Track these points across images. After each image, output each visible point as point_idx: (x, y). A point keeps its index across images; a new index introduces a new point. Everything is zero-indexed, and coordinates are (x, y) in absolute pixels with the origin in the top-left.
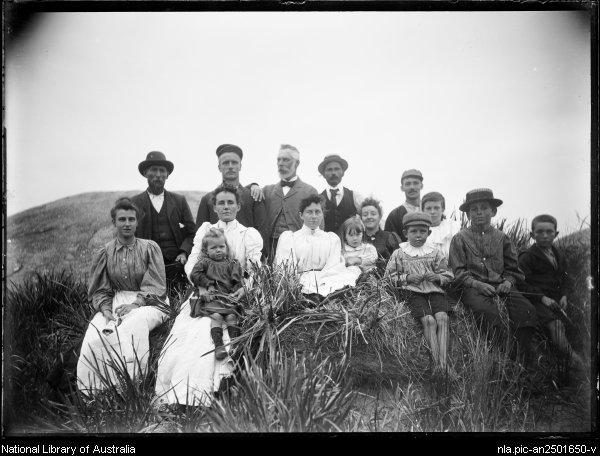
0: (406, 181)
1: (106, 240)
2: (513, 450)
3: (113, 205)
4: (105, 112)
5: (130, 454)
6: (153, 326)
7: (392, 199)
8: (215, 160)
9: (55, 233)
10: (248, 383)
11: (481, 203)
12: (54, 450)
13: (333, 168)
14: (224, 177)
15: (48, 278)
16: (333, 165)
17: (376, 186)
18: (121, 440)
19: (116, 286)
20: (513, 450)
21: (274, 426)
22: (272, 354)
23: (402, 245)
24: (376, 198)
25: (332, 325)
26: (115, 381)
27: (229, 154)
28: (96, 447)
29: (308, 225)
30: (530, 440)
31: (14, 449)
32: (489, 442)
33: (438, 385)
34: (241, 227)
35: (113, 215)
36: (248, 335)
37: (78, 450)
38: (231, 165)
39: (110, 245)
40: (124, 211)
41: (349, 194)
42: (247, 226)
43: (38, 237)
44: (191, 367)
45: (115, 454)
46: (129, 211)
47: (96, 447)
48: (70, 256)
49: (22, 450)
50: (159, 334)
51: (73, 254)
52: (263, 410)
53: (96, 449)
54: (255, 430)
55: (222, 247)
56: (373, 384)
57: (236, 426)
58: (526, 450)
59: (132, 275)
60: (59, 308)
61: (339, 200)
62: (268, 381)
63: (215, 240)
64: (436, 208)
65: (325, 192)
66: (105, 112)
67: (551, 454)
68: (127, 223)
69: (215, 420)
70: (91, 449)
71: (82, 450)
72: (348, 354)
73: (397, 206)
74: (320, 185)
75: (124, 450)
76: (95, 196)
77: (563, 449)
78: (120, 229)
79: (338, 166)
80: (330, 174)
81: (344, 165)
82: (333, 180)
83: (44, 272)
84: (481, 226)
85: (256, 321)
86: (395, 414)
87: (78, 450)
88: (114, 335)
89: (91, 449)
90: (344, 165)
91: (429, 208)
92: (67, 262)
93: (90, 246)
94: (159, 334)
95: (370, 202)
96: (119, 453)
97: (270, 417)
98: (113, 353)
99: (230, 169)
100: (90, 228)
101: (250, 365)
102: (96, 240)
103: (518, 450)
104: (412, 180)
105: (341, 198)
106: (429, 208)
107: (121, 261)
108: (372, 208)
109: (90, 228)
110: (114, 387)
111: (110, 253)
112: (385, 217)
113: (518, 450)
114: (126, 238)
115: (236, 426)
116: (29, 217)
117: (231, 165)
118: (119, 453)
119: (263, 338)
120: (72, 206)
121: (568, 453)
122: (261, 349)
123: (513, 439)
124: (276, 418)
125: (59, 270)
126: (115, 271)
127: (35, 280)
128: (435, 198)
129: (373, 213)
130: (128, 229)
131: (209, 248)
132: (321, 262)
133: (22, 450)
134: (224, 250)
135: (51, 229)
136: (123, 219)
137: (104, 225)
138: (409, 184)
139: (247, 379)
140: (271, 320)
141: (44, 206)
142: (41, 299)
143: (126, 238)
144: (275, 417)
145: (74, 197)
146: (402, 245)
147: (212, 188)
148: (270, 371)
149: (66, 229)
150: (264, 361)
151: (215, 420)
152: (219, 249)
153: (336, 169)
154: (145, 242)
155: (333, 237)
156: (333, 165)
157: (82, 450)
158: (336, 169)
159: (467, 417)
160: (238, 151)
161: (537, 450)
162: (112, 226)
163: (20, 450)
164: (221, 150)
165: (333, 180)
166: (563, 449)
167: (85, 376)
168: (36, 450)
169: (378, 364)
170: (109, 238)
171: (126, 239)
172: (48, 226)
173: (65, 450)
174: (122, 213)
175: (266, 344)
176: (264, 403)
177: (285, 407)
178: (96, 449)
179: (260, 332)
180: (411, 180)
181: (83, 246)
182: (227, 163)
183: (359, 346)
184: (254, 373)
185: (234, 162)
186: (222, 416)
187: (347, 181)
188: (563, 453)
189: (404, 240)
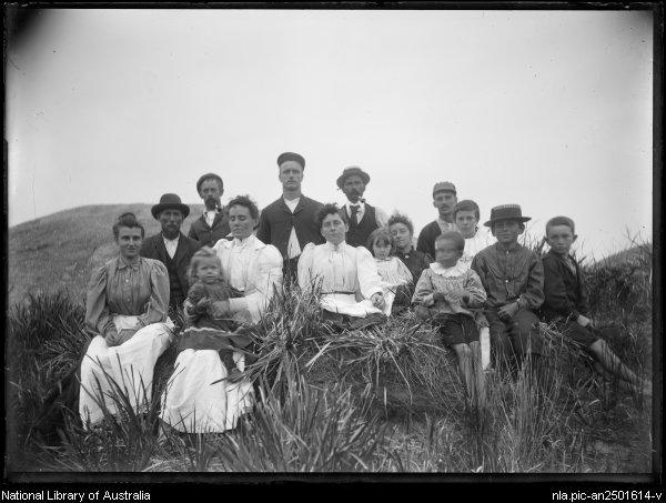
0: (437, 196)
1: (107, 258)
2: (569, 496)
3: (114, 220)
4: (116, 123)
5: (144, 501)
6: (158, 353)
7: (423, 215)
8: (276, 170)
9: (50, 250)
10: (264, 416)
11: (509, 219)
12: (59, 496)
13: (353, 181)
14: (284, 187)
15: (43, 300)
16: (354, 179)
17: (403, 197)
18: (133, 482)
19: (113, 308)
20: (569, 496)
21: (293, 464)
22: (292, 384)
23: (432, 265)
24: (402, 213)
25: (355, 351)
26: (113, 410)
27: (291, 165)
28: (107, 493)
29: (332, 241)
30: (589, 486)
31: (15, 496)
32: (542, 487)
33: (475, 423)
34: (260, 244)
35: (116, 232)
36: (264, 363)
37: (86, 496)
38: (291, 174)
39: (111, 263)
40: (128, 229)
41: (370, 211)
42: (355, 246)
43: (31, 255)
44: (207, 395)
45: (128, 501)
46: (134, 229)
47: (107, 493)
48: (67, 276)
49: (25, 496)
50: (165, 364)
51: (70, 273)
52: (280, 446)
53: (107, 495)
54: (271, 468)
55: (213, 267)
56: (402, 417)
57: (251, 463)
58: (583, 496)
59: (135, 299)
60: (61, 330)
61: (359, 218)
62: (285, 417)
63: (207, 259)
64: (469, 218)
65: (345, 207)
66: (116, 123)
67: (612, 501)
68: (131, 242)
69: (227, 456)
70: (101, 495)
71: (92, 496)
72: (374, 381)
73: (432, 221)
74: (341, 200)
75: (138, 496)
76: (96, 209)
77: (626, 496)
78: (123, 247)
79: (359, 179)
80: (350, 188)
81: (365, 178)
82: (354, 195)
83: (38, 293)
84: (507, 244)
85: (272, 347)
86: (416, 454)
87: (86, 496)
88: (118, 359)
89: (101, 495)
90: (365, 178)
91: (461, 219)
92: (64, 283)
93: (88, 265)
94: (165, 364)
95: (396, 219)
96: (132, 500)
97: (288, 453)
98: (114, 386)
99: (291, 178)
100: (91, 245)
101: (266, 395)
102: (95, 258)
103: (574, 496)
104: (444, 194)
105: (362, 215)
106: (461, 219)
107: (123, 282)
108: (399, 225)
109: (91, 245)
110: (114, 418)
111: (112, 273)
112: (417, 234)
113: (574, 496)
114: (130, 258)
115: (251, 463)
116: (21, 232)
117: (291, 174)
118: (132, 500)
119: (280, 368)
120: (69, 220)
121: (630, 500)
122: (278, 378)
123: (570, 484)
124: (295, 455)
125: (53, 291)
126: (115, 293)
127: (28, 303)
128: (470, 207)
129: (402, 231)
130: (132, 248)
131: (199, 268)
132: (358, 283)
133: (25, 496)
134: (216, 273)
135: (46, 246)
136: (127, 238)
137: (104, 242)
138: (440, 199)
139: (262, 412)
140: (289, 347)
141: (37, 221)
142: (34, 323)
143: (130, 258)
144: (294, 454)
145: (71, 211)
146: (432, 265)
147: (278, 196)
148: (288, 403)
149: (62, 245)
150: (282, 392)
151: (227, 456)
152: (210, 270)
153: (357, 183)
154: (150, 261)
155: (363, 250)
156: (354, 179)
157: (92, 496)
158: (357, 183)
159: (511, 457)
160: (301, 161)
161: (596, 496)
162: (114, 244)
163: (22, 496)
164: (283, 159)
165: (354, 195)
166: (626, 496)
167: (89, 409)
168: (40, 496)
169: (407, 396)
170: (109, 256)
171: (130, 258)
172: (42, 243)
173: (73, 496)
174: (125, 231)
175: (283, 373)
176: (282, 440)
177: (305, 444)
178: (107, 495)
179: (277, 360)
180: (444, 195)
181: (82, 265)
182: (288, 171)
183: (387, 373)
184: (273, 407)
185: (295, 171)
186: (234, 452)
187: (371, 195)
188: (625, 500)
189: (433, 259)
